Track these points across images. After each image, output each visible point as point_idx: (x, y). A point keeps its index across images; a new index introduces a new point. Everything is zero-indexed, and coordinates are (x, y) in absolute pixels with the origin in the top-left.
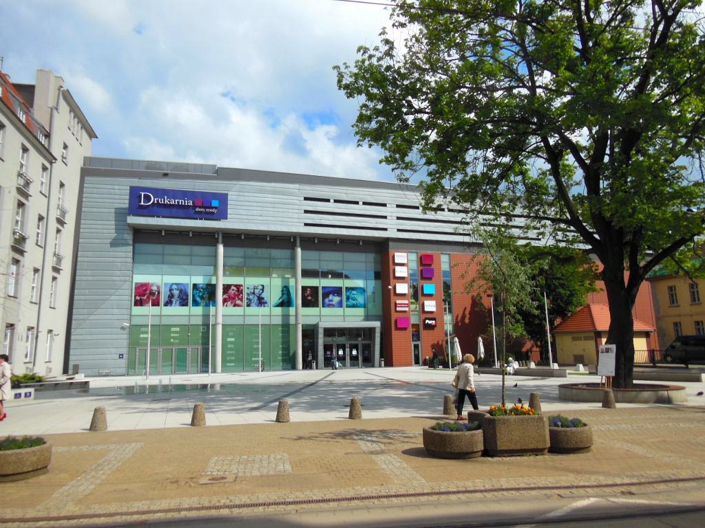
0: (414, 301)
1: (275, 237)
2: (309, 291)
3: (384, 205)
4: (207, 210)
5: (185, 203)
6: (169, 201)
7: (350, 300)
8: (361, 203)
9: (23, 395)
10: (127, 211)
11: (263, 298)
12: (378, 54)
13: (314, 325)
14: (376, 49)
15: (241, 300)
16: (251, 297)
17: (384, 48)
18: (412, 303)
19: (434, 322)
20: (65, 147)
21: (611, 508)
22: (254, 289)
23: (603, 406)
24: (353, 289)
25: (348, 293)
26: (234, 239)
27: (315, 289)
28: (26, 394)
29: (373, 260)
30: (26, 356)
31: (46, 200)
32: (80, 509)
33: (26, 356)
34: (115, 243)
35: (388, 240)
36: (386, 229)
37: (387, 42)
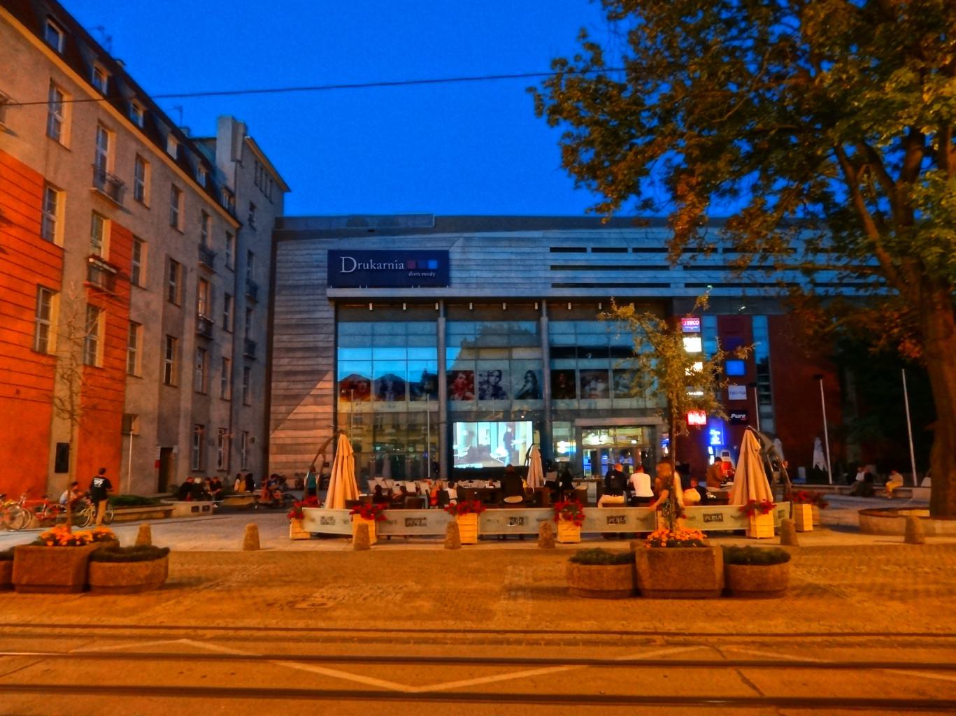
2: (562, 377)
4: (423, 274)
5: (395, 266)
6: (376, 266)
7: (620, 388)
9: (201, 509)
10: (326, 282)
11: (500, 388)
12: (581, 65)
14: (578, 58)
15: (472, 391)
16: (485, 387)
17: (588, 55)
19: (744, 416)
20: (252, 207)
21: (764, 659)
22: (488, 376)
23: (906, 541)
24: (623, 371)
25: (617, 378)
26: (457, 308)
27: (570, 374)
28: (204, 507)
30: (220, 463)
32: (277, 623)
33: (220, 463)
34: (577, 187)
36: (667, 285)
37: (592, 47)
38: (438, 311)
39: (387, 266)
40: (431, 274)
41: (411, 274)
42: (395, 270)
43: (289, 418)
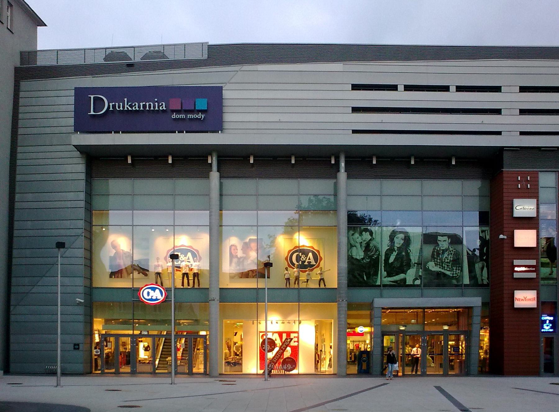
0: (547, 260)
1: (304, 158)
3: (497, 89)
4: (190, 116)
5: (154, 107)
6: (131, 106)
8: (401, 88)
13: (62, 376)
18: (544, 265)
29: (477, 193)
31: (89, 224)
35: (501, 150)
38: (211, 164)
39: (144, 106)
40: (200, 116)
41: (174, 116)
42: (181, 118)
43: (33, 291)
